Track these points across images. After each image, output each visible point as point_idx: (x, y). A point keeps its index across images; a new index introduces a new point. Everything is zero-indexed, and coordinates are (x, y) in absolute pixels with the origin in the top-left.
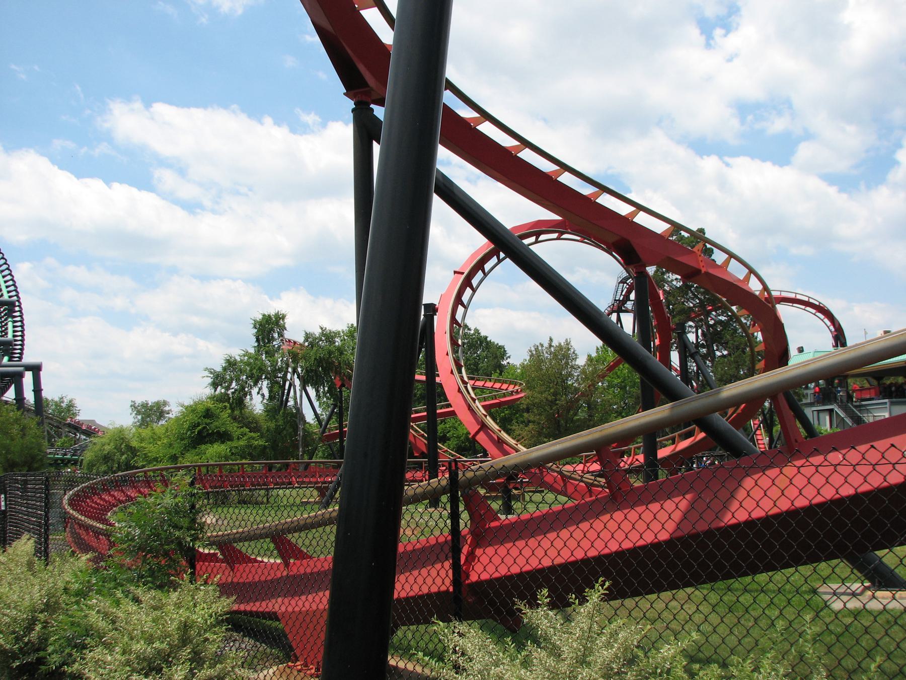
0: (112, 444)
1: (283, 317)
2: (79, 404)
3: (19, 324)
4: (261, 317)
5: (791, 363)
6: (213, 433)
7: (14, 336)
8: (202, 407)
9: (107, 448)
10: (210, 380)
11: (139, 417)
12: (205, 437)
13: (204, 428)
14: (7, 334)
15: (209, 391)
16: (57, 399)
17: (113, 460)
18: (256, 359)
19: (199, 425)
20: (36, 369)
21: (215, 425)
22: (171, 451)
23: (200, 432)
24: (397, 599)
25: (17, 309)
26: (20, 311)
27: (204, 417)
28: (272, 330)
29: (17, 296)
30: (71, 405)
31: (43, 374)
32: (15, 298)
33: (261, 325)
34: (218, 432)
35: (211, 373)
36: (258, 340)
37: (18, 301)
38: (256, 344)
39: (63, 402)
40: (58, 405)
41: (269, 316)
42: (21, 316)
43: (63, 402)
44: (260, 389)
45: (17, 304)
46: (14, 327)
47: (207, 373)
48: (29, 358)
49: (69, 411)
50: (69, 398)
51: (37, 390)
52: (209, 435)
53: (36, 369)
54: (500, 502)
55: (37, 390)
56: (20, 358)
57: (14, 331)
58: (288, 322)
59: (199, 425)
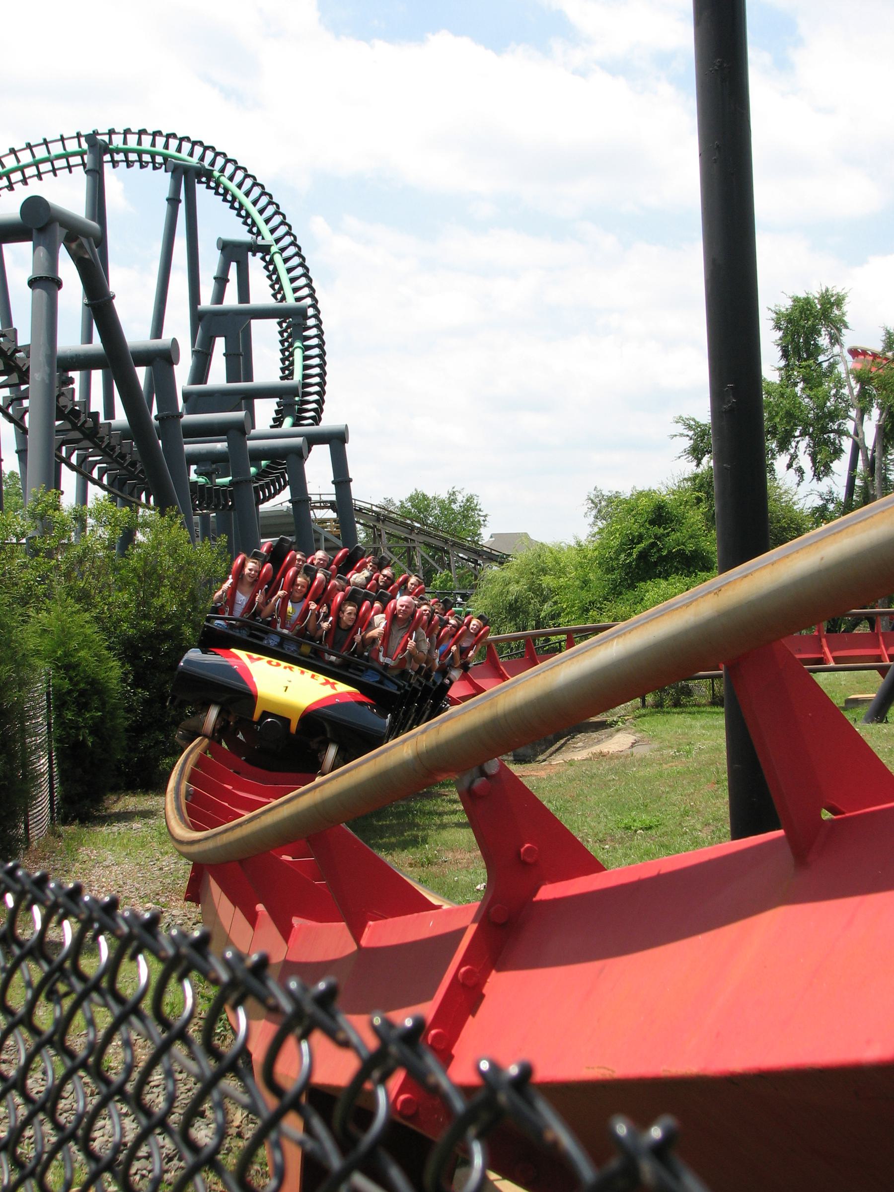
0: (523, 581)
1: (839, 302)
2: (485, 504)
3: (316, 351)
4: (789, 303)
5: (321, 424)
6: (671, 556)
7: (305, 377)
8: (644, 501)
9: (514, 588)
10: (687, 443)
11: (601, 524)
12: (655, 564)
13: (653, 545)
14: (292, 373)
15: (689, 468)
16: (444, 496)
17: (526, 613)
18: (782, 395)
19: (641, 538)
20: (337, 440)
21: (674, 539)
22: (584, 594)
23: (643, 556)
24: (410, 810)
25: (311, 322)
26: (318, 326)
27: (652, 522)
28: (815, 331)
29: (312, 296)
30: (469, 507)
31: (350, 448)
32: (308, 301)
33: (790, 321)
34: (681, 553)
35: (690, 427)
36: (785, 355)
37: (314, 306)
38: (783, 363)
39: (454, 501)
40: (445, 507)
41: (807, 301)
42: (320, 336)
43: (454, 501)
44: (794, 457)
45: (311, 312)
46: (306, 358)
47: (680, 428)
48: (330, 421)
49: (466, 517)
50: (467, 493)
51: (342, 481)
52: (662, 559)
53: (337, 440)
54: (131, 632)
55: (342, 481)
56: (317, 420)
57: (306, 367)
58: (850, 311)
59: (641, 538)
